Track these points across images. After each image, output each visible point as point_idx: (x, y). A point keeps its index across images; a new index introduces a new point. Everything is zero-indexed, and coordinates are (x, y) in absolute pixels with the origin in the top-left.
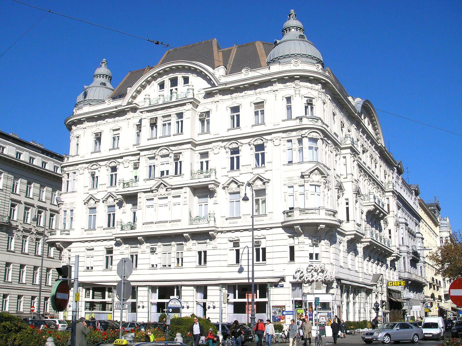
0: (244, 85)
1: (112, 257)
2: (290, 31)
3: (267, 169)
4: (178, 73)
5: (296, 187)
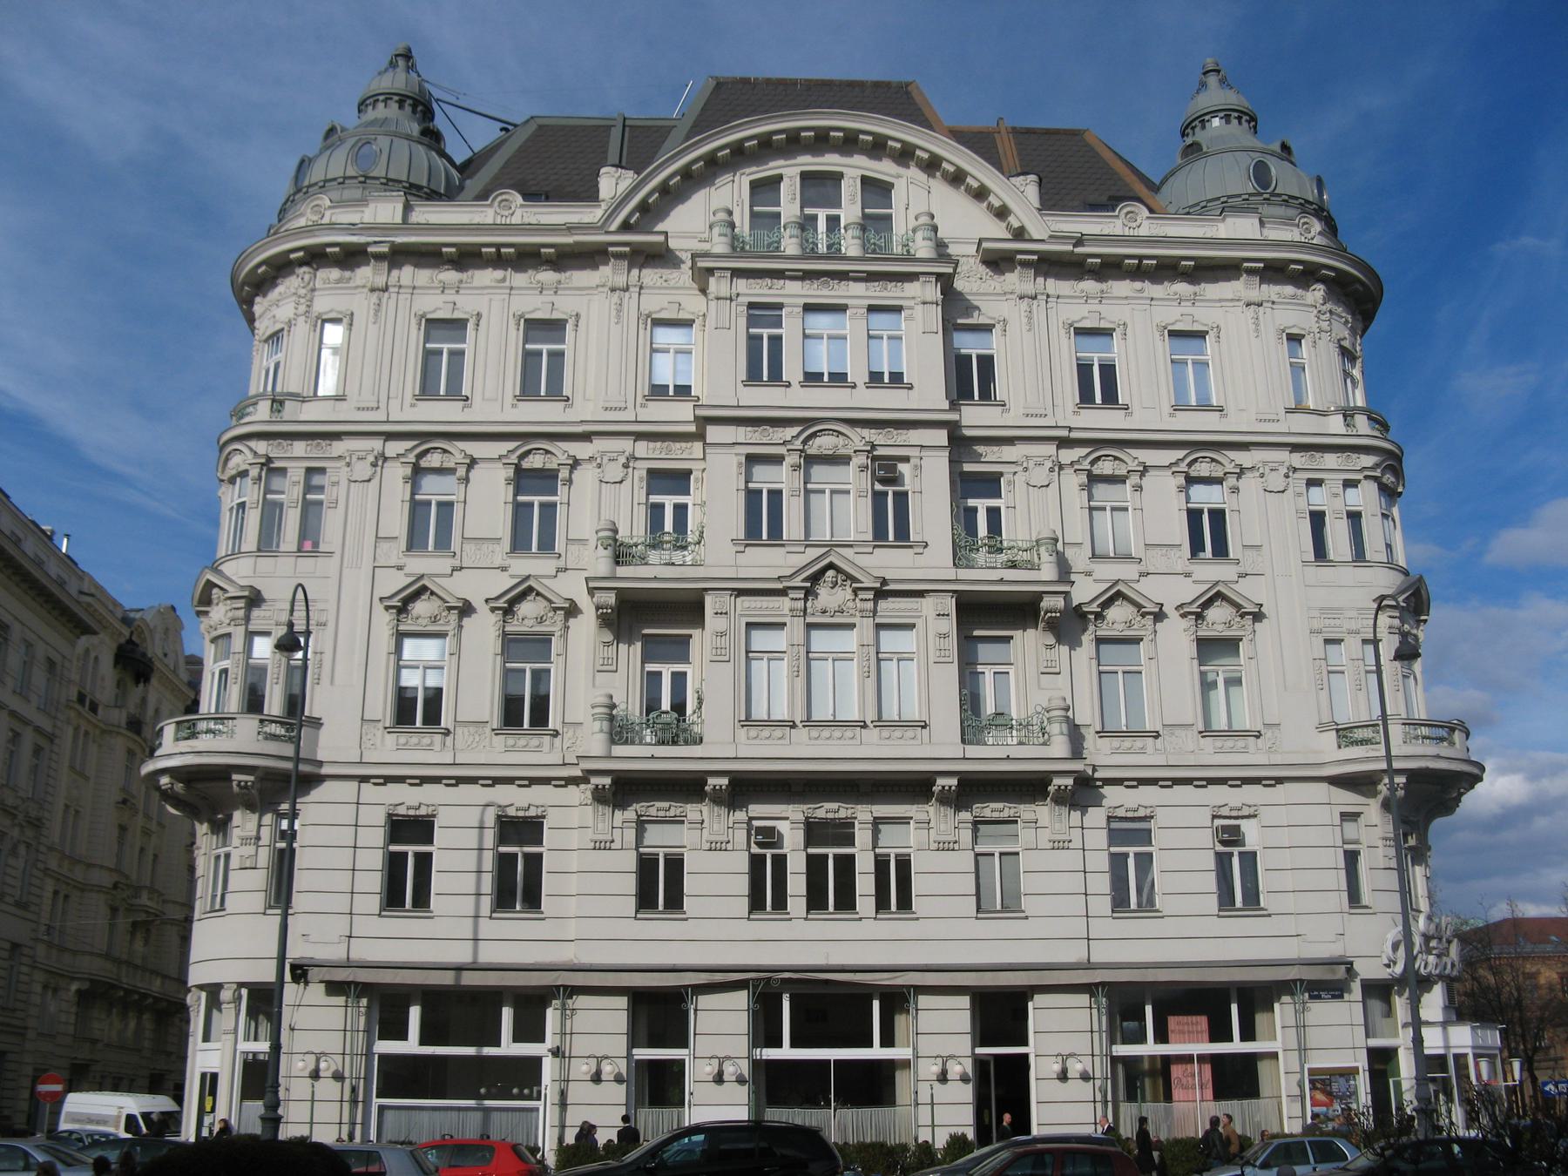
2: (1203, 127)
4: (781, 162)
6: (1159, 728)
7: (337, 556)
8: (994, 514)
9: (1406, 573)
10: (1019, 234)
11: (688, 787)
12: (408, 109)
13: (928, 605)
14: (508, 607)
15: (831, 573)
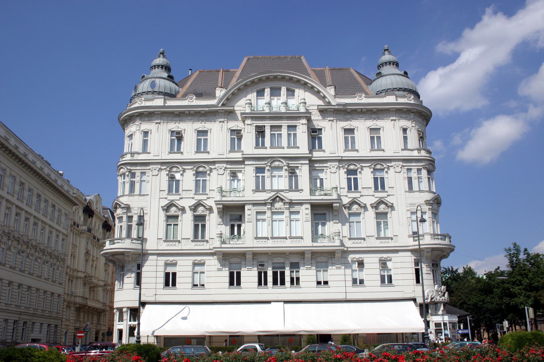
0: (362, 109)
6: (365, 237)
7: (150, 195)
9: (435, 193)
10: (329, 103)
12: (164, 69)
13: (305, 206)
14: (194, 208)
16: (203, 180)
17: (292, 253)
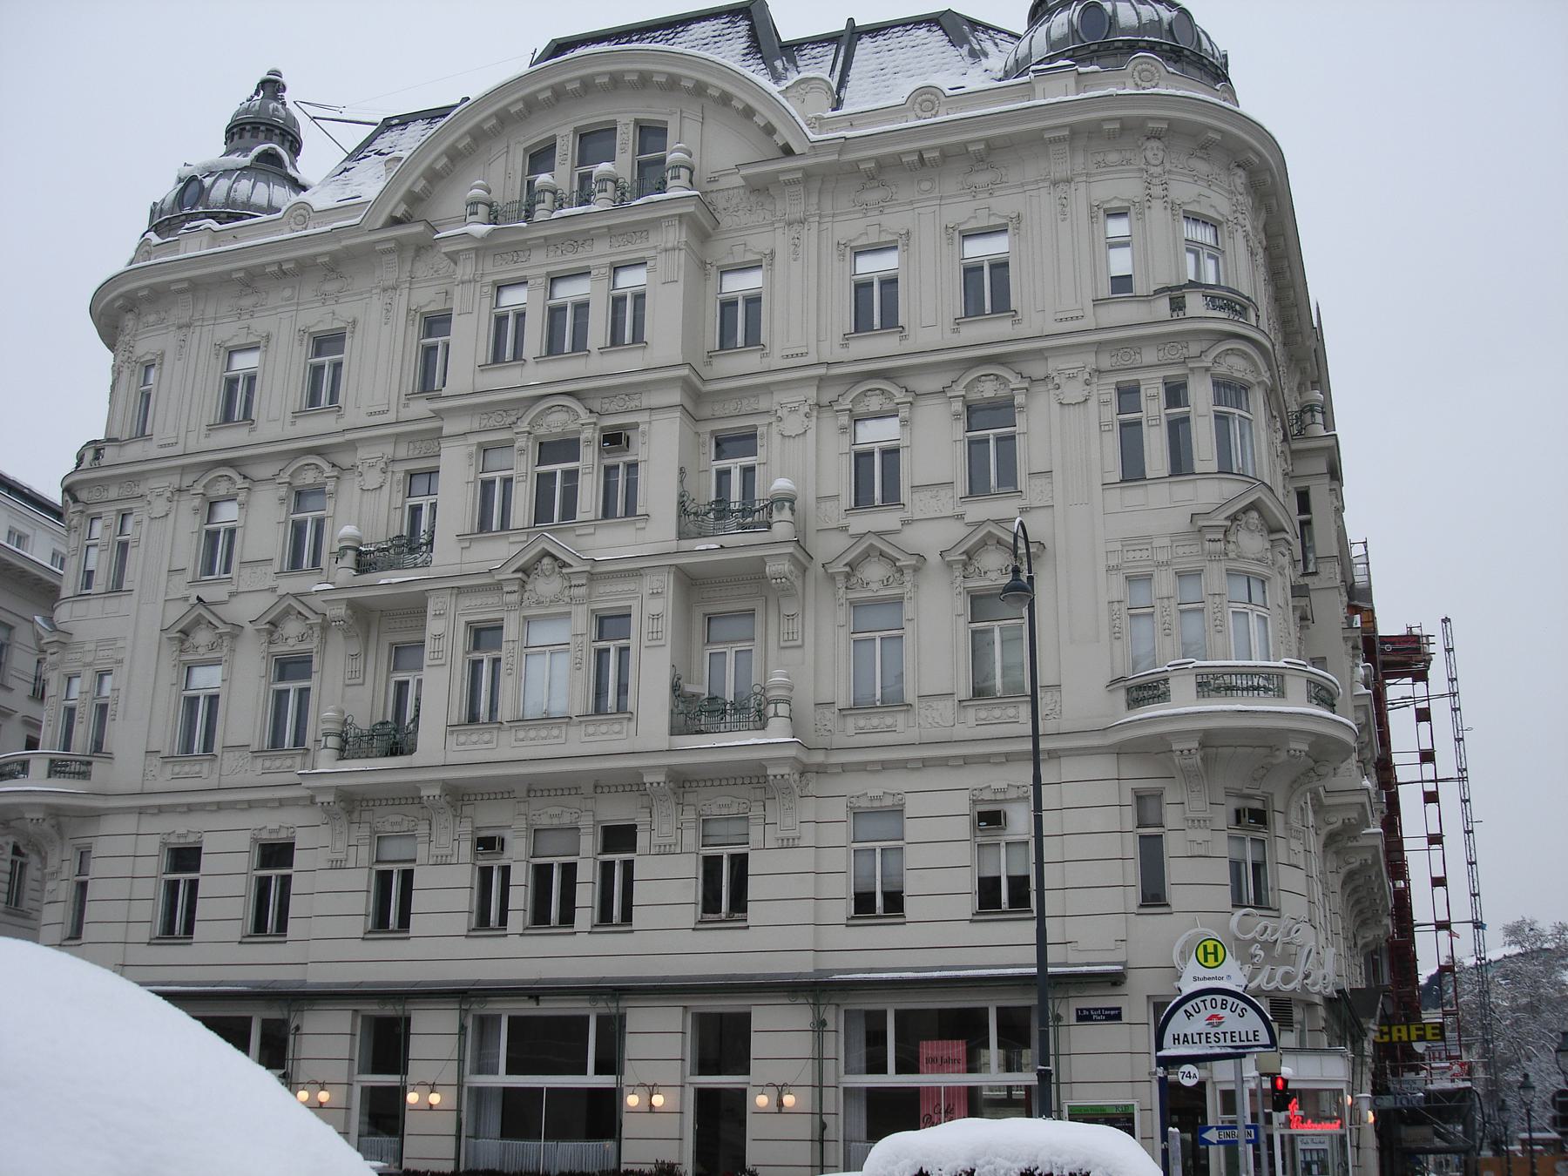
1: (193, 885)
3: (907, 515)
5: (1165, 583)
8: (748, 471)
11: (407, 798)
13: (649, 583)
15: (546, 561)
16: (999, 439)
17: (602, 785)
